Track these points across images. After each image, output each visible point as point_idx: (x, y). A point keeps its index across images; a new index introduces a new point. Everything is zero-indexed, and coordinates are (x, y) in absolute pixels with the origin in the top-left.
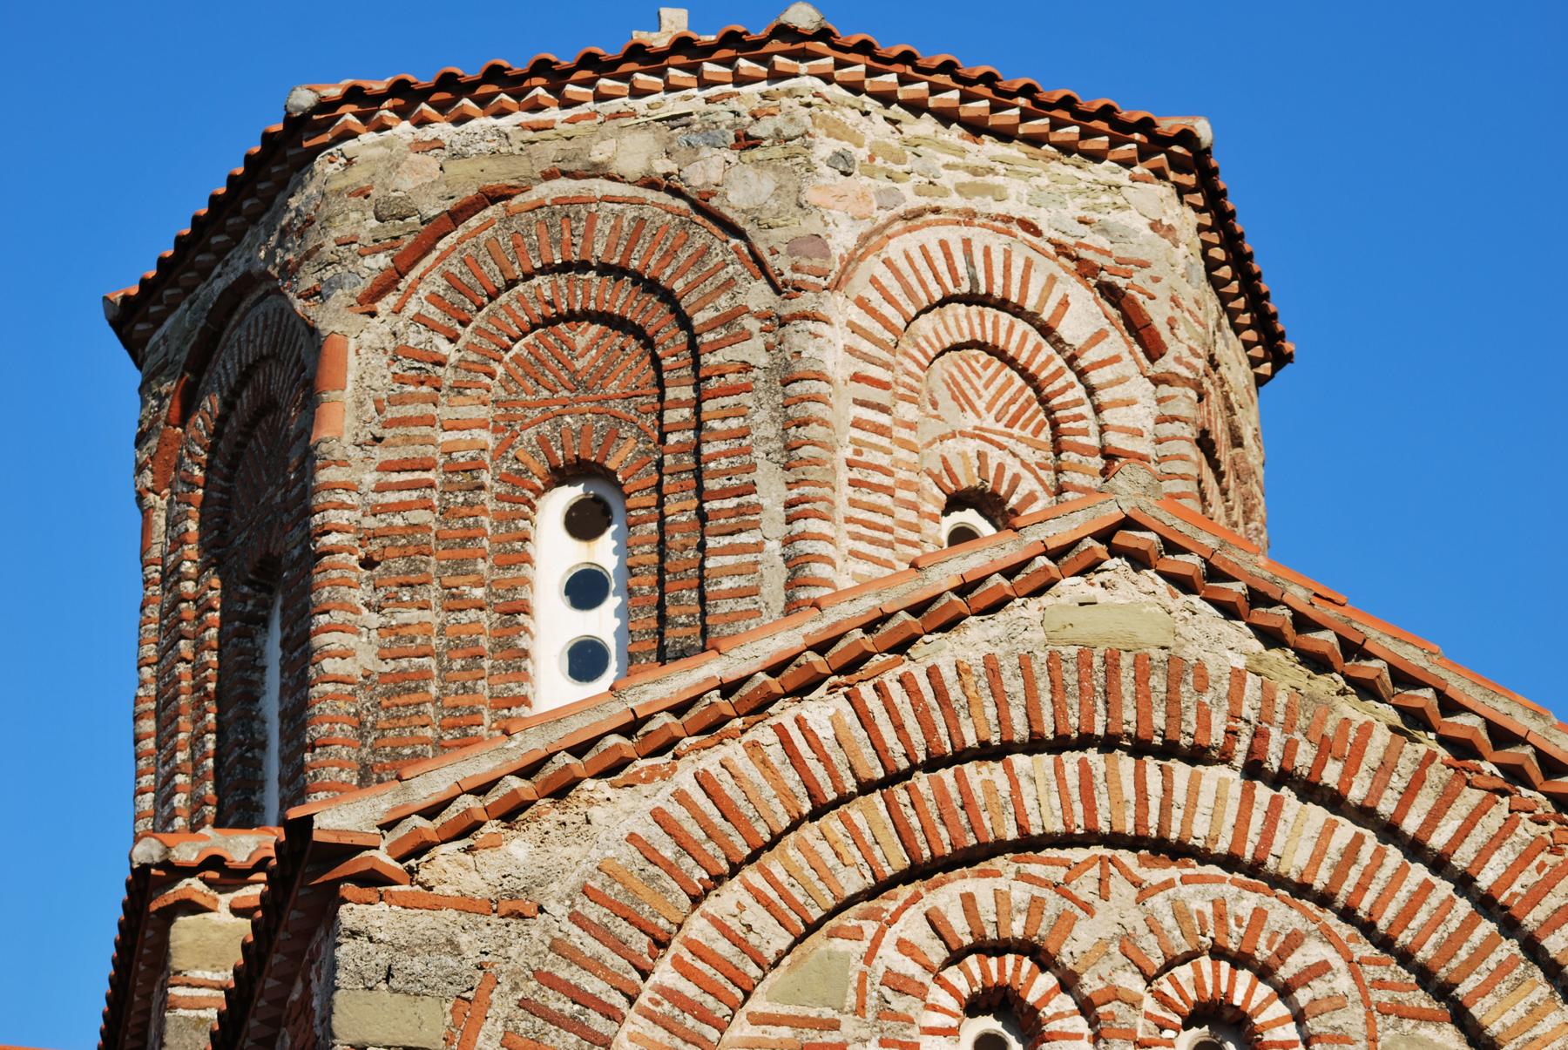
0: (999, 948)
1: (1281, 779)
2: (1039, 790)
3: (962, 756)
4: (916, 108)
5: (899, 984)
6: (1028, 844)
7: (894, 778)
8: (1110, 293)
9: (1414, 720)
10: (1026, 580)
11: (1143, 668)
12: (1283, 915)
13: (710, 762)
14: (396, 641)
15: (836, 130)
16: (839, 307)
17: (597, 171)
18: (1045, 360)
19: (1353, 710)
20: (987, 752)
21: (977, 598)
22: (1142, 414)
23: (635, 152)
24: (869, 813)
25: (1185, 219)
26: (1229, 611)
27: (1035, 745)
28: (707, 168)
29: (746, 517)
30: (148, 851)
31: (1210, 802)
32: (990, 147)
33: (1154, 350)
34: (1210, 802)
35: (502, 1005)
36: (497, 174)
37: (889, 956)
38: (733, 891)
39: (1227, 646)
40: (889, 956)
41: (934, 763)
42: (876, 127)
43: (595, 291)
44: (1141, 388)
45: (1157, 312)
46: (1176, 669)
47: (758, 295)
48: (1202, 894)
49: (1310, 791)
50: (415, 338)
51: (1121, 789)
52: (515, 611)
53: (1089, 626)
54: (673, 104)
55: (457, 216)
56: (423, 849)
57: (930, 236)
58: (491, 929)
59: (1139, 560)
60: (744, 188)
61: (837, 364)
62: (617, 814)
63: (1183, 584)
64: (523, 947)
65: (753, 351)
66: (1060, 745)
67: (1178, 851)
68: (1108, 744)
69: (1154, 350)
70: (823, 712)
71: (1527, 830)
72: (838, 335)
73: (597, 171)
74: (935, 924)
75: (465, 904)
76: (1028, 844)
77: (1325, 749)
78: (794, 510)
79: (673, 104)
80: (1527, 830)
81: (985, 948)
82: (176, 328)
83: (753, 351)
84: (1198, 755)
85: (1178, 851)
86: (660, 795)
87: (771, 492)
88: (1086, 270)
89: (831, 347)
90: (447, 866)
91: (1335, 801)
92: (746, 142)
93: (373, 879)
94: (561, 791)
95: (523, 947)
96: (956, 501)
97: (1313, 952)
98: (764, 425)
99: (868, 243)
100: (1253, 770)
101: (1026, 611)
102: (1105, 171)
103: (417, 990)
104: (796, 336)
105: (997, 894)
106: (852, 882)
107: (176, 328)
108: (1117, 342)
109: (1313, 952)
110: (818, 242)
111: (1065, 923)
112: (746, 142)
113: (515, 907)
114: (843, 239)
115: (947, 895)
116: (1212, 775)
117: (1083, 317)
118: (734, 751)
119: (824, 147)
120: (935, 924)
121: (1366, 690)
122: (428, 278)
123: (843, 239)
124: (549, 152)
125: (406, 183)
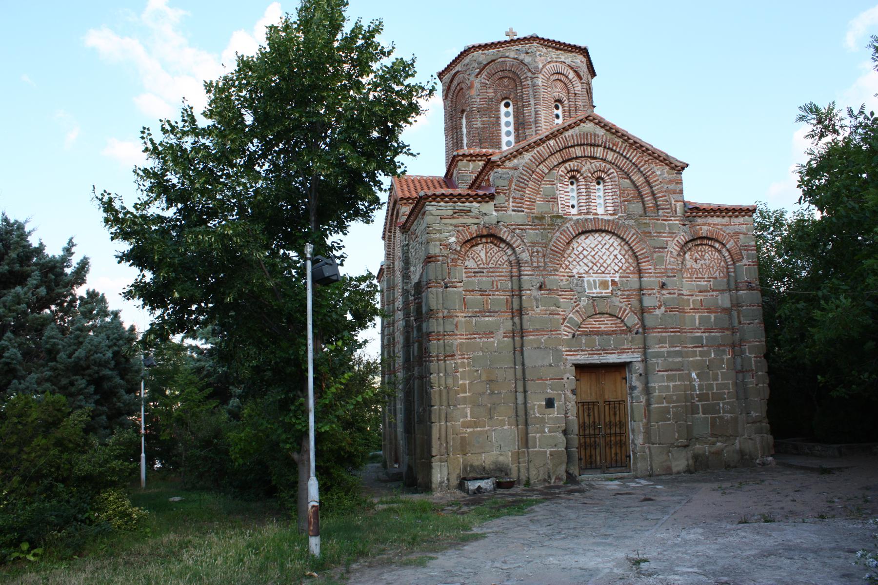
0: (571, 171)
1: (609, 148)
2: (578, 151)
3: (569, 147)
4: (550, 47)
5: (561, 176)
6: (577, 158)
7: (561, 150)
8: (575, 71)
9: (626, 141)
10: (576, 124)
11: (591, 135)
12: (608, 166)
13: (538, 149)
14: (483, 122)
15: (539, 51)
16: (541, 76)
17: (507, 57)
18: (567, 81)
19: (617, 140)
20: (572, 146)
21: (570, 127)
22: (579, 88)
23: (512, 55)
24: (558, 155)
25: (584, 60)
26: (602, 127)
27: (578, 145)
28: (522, 57)
29: (529, 105)
30: (455, 153)
31: (599, 152)
32: (559, 52)
33: (581, 79)
34: (599, 152)
35: (515, 180)
36: (493, 58)
37: (560, 172)
38: (541, 166)
39: (601, 132)
40: (560, 172)
41: (566, 148)
42: (544, 50)
43: (507, 74)
44: (579, 84)
45: (582, 74)
46: (595, 135)
47: (529, 74)
48: (597, 164)
49: (612, 150)
50: (483, 81)
51: (589, 151)
52: (498, 118)
53: (584, 130)
54: (517, 47)
55: (488, 64)
56: (504, 161)
57: (552, 65)
58: (513, 171)
59: (591, 121)
60: (528, 59)
61: (540, 84)
62: (527, 156)
63: (596, 124)
64: (517, 173)
65: (529, 82)
66: (581, 145)
67: (595, 158)
68: (587, 145)
69: (581, 79)
70: (552, 142)
71: (638, 155)
72: (540, 80)
73: (507, 57)
74: (566, 168)
75: (509, 168)
76: (577, 158)
77: (614, 145)
78: (536, 104)
79: (517, 47)
80: (638, 155)
81: (571, 171)
82: (447, 77)
83: (529, 82)
84: (598, 146)
85: (595, 158)
86: (532, 153)
87: (532, 102)
88: (572, 68)
89: (539, 82)
90: (508, 164)
91: (615, 151)
92: (527, 53)
93: (499, 166)
94: (521, 153)
95: (517, 173)
96: (556, 101)
97: (612, 170)
98: (531, 92)
99: (544, 66)
100: (605, 147)
101: (577, 128)
102: (574, 54)
103: (504, 179)
104: (535, 80)
105: (573, 164)
106: (556, 163)
107: (447, 77)
108: (576, 78)
109: (612, 170)
110: (537, 67)
111: (581, 168)
112: (527, 53)
113: (515, 168)
114: (541, 66)
115: (567, 165)
116: (599, 149)
117: (571, 75)
118: (541, 147)
119: (538, 53)
120: (566, 168)
121: (619, 137)
122: (484, 74)
123: (541, 66)
124: (500, 55)
125: (481, 59)
